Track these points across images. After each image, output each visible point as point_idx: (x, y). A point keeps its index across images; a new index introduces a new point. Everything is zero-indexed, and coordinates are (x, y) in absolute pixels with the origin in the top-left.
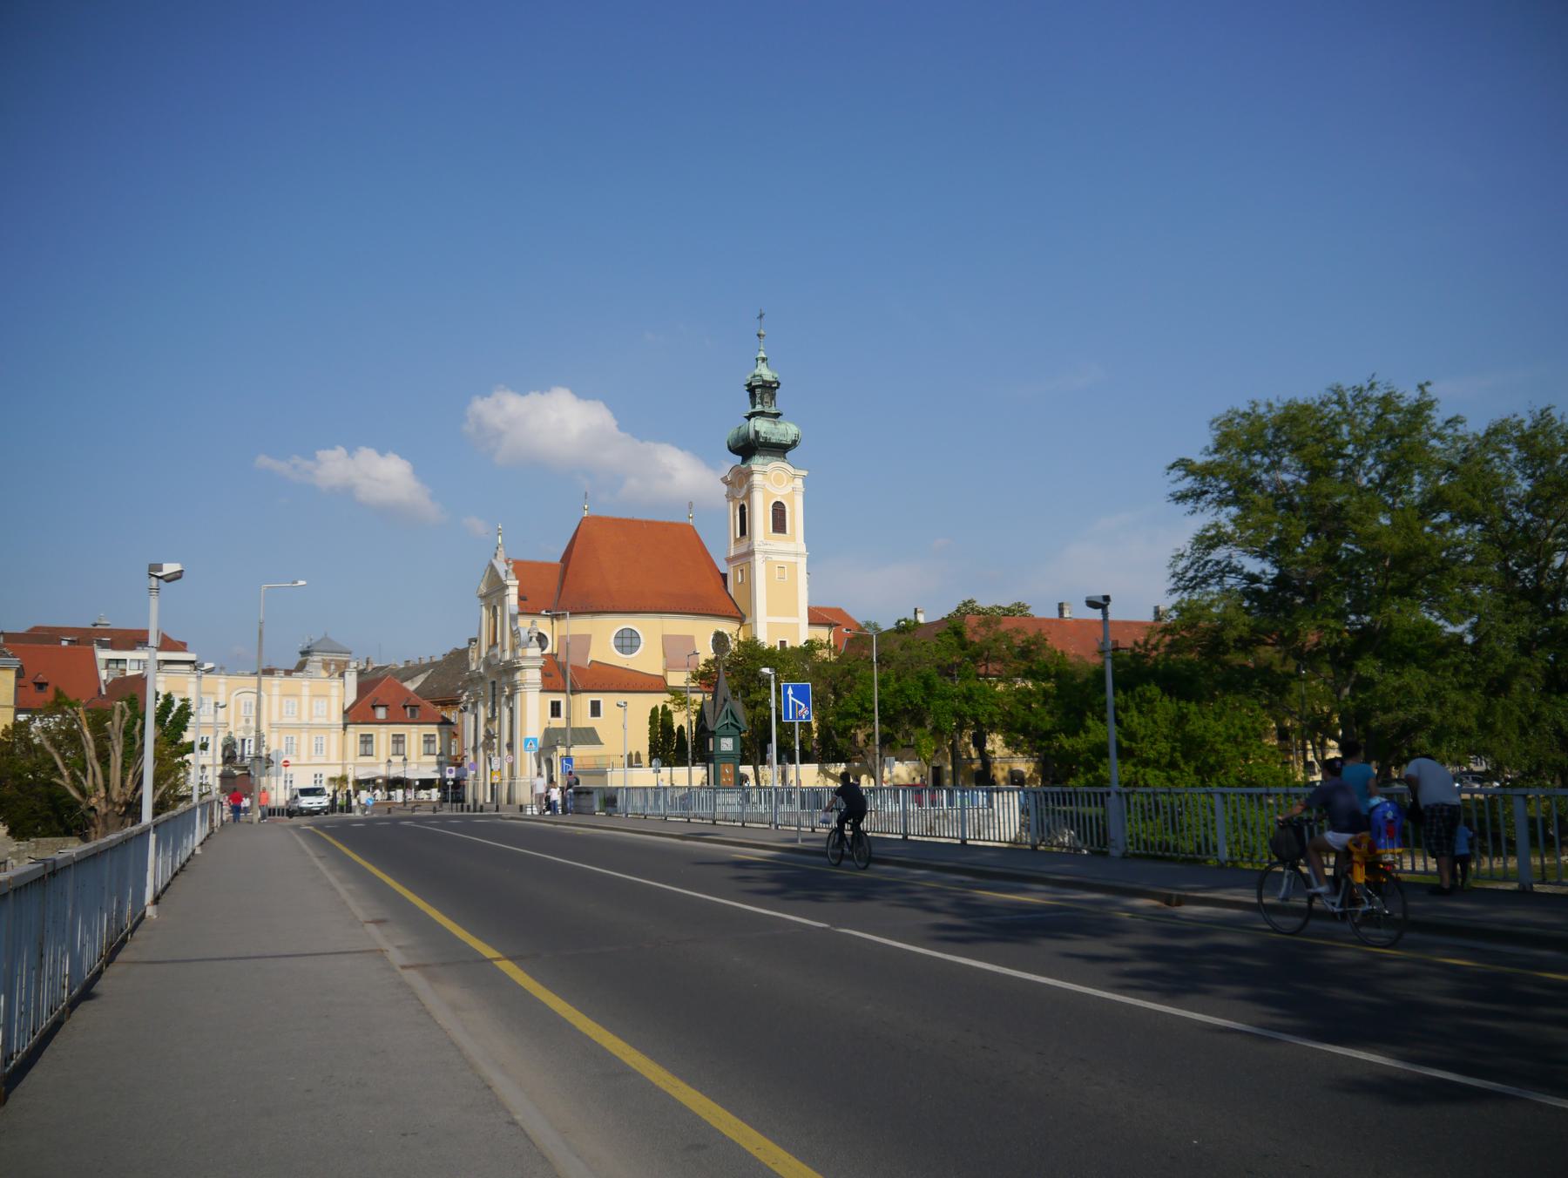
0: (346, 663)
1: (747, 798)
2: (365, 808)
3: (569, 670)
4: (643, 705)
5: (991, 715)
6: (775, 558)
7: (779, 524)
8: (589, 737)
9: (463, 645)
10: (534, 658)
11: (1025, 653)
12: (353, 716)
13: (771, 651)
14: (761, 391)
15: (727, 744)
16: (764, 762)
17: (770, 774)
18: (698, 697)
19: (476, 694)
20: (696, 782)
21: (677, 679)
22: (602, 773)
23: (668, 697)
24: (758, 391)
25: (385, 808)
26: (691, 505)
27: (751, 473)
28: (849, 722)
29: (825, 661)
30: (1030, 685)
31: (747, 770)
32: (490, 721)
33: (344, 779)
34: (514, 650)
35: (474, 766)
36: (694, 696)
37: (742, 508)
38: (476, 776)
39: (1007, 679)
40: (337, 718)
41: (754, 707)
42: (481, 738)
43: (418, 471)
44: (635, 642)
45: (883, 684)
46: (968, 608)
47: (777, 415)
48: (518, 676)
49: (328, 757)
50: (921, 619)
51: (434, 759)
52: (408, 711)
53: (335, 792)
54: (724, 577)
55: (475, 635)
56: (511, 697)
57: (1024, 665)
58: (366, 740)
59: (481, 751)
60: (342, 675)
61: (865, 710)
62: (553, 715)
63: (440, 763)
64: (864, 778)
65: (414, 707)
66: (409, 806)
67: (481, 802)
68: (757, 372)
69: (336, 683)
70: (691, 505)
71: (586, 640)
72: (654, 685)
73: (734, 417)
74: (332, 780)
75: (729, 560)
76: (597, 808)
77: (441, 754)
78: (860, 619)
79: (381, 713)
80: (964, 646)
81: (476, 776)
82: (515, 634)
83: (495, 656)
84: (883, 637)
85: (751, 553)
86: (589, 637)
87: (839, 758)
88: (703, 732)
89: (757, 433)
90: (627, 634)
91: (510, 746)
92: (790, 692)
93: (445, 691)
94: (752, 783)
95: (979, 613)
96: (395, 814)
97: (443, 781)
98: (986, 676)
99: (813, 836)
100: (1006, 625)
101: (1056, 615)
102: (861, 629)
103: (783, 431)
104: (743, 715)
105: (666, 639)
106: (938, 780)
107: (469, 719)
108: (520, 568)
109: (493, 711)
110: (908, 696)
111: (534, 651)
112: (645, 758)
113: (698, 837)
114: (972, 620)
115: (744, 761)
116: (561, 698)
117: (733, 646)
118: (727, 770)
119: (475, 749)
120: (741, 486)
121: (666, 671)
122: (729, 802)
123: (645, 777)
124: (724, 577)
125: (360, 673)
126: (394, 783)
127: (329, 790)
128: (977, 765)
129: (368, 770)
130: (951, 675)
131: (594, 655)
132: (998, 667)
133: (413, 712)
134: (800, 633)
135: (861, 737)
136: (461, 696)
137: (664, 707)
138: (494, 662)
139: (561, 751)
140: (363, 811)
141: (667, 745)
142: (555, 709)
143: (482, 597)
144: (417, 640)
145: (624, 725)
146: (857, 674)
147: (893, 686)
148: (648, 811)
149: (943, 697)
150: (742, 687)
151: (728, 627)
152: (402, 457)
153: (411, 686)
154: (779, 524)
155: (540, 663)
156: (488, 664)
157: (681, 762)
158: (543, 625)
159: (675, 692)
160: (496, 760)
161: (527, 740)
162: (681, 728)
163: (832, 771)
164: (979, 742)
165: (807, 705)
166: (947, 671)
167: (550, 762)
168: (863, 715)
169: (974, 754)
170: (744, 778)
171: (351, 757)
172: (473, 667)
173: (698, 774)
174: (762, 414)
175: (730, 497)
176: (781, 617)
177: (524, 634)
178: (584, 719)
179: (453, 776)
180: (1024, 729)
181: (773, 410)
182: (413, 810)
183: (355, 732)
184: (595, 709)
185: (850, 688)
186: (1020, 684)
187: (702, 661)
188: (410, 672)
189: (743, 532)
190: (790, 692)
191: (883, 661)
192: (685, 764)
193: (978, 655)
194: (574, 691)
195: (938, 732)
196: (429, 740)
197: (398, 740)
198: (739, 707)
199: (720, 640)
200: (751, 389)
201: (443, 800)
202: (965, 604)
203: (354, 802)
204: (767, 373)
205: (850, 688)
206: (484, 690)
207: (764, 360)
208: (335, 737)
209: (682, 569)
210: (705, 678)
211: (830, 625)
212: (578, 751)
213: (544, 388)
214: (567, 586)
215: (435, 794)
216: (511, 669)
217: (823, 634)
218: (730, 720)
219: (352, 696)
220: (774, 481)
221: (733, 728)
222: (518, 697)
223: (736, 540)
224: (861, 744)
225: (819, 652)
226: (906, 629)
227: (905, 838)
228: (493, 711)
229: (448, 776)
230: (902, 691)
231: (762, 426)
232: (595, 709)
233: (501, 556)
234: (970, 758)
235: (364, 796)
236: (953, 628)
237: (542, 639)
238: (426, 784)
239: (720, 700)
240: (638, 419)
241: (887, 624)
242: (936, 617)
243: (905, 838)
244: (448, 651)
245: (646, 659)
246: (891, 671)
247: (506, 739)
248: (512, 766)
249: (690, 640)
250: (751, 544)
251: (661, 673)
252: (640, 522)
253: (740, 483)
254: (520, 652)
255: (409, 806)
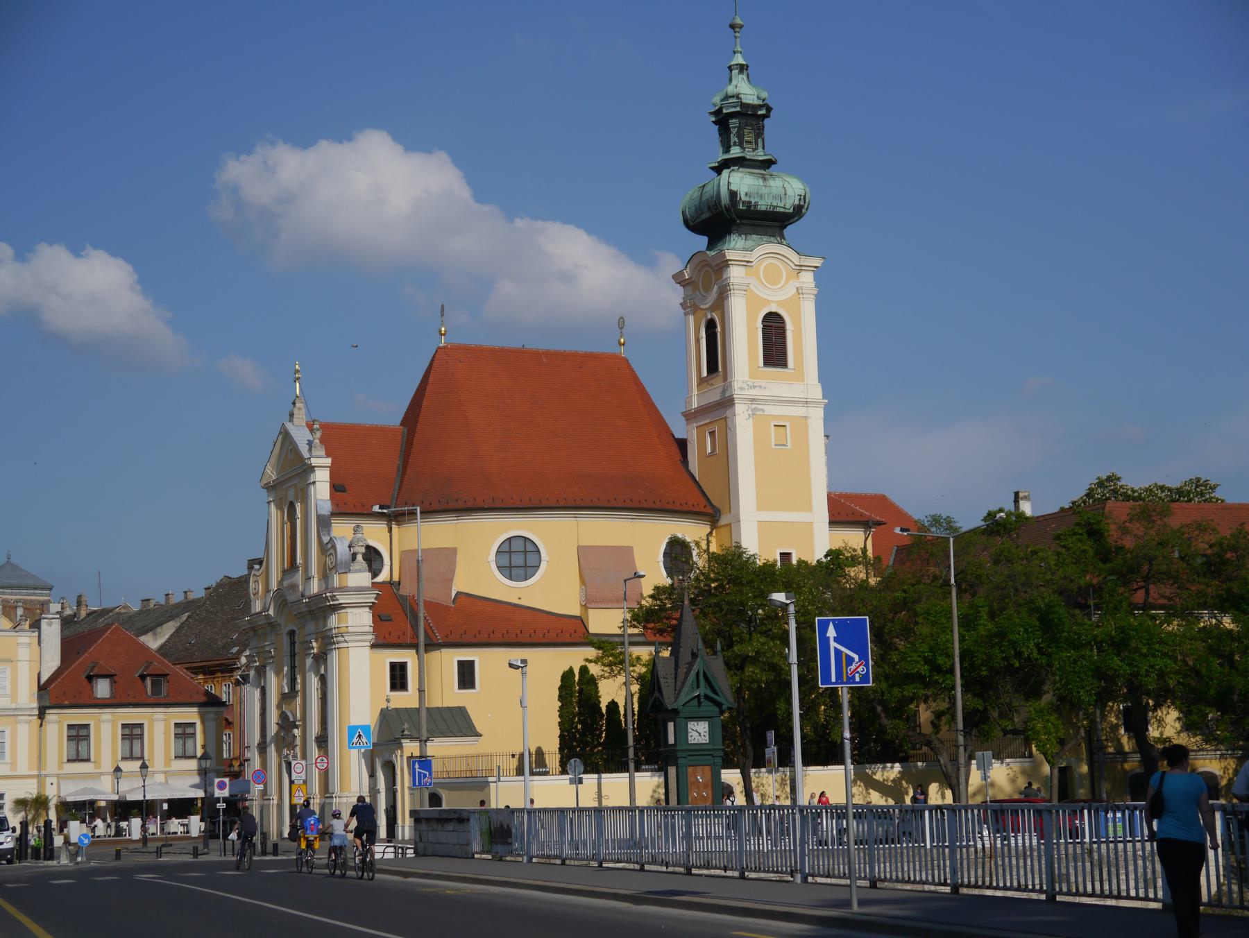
0: (44, 606)
1: (734, 824)
2: (74, 850)
3: (422, 613)
4: (550, 665)
5: (1162, 675)
6: (770, 410)
7: (775, 348)
8: (456, 723)
9: (239, 571)
10: (359, 590)
11: (1215, 566)
12: (52, 695)
13: (768, 568)
14: (739, 123)
15: (699, 732)
16: (760, 762)
17: (769, 784)
18: (645, 653)
19: (262, 653)
20: (643, 800)
21: (606, 622)
22: (483, 785)
23: (591, 652)
24: (734, 123)
25: (112, 850)
26: (621, 323)
27: (725, 264)
28: (909, 690)
29: (863, 586)
30: (1227, 622)
31: (731, 776)
32: (286, 698)
33: (40, 803)
34: (325, 576)
35: (262, 775)
36: (637, 651)
37: (711, 325)
38: (264, 793)
39: (1186, 614)
40: (27, 698)
41: (741, 668)
42: (273, 729)
43: (150, 282)
44: (531, 559)
45: (966, 622)
46: (1108, 484)
47: (767, 164)
48: (333, 621)
49: (13, 765)
50: (1026, 508)
51: (193, 765)
52: (147, 685)
53: (24, 825)
54: (682, 444)
55: (259, 554)
56: (322, 658)
57: (1213, 588)
58: (79, 734)
59: (272, 751)
60: (36, 625)
61: (936, 669)
62: (394, 687)
63: (203, 772)
64: (933, 788)
65: (159, 678)
66: (152, 846)
67: (273, 837)
68: (731, 89)
69: (26, 638)
70: (621, 323)
71: (449, 555)
72: (568, 632)
73: (691, 166)
74: (21, 804)
75: (690, 416)
76: (476, 846)
77: (205, 757)
78: (918, 510)
79: (103, 689)
80: (1105, 555)
81: (264, 793)
82: (327, 549)
83: (294, 587)
84: (966, 540)
85: (727, 402)
86: (454, 551)
87: (886, 757)
88: (654, 706)
89: (733, 195)
90: (517, 546)
91: (323, 741)
92: (831, 632)
93: (217, 651)
94: (740, 800)
95: (1128, 498)
96: (128, 860)
97: (209, 801)
98: (1146, 606)
99: (873, 894)
100: (1179, 518)
101: (1010, 506)
102: (922, 528)
103: (782, 189)
104: (725, 682)
105: (584, 553)
106: (1065, 791)
107: (252, 695)
108: (334, 437)
109: (293, 681)
110: (1013, 644)
111: (359, 578)
112: (553, 760)
113: (663, 898)
114: (1118, 511)
115: (729, 765)
116: (407, 657)
117: (700, 561)
118: (700, 776)
119: (262, 747)
120: (708, 289)
121: (585, 607)
122: (710, 833)
123: (555, 791)
124: (682, 444)
125: (66, 622)
126: (123, 809)
127: (14, 821)
128: (1133, 764)
129: (82, 785)
130: (1084, 607)
131: (463, 583)
132: (1168, 592)
133: (156, 685)
134: (817, 540)
135: (925, 715)
136: (237, 657)
137: (584, 670)
138: (291, 598)
139: (411, 748)
140: (73, 856)
141: (590, 738)
142: (398, 677)
143: (270, 488)
144: (161, 563)
145: (515, 703)
146: (919, 608)
147: (986, 626)
148: (567, 851)
149: (1076, 645)
150: (719, 633)
151: (692, 531)
152: (113, 253)
153: (153, 642)
154: (775, 348)
155: (371, 598)
156: (281, 599)
157: (618, 765)
158: (375, 534)
159: (603, 643)
160: (298, 766)
161: (352, 729)
162: (613, 705)
163: (878, 777)
164: (1136, 723)
165: (863, 657)
166: (1078, 600)
167: (390, 768)
168: (933, 678)
169: (1127, 743)
170: (729, 791)
171: (52, 765)
172: (257, 607)
173: (648, 785)
174: (741, 162)
175: (689, 306)
176: (782, 511)
177: (342, 549)
178: (447, 693)
179: (226, 793)
180: (1222, 702)
181: (760, 155)
182: (159, 853)
183: (59, 721)
184: (466, 675)
185: (906, 632)
186: (1206, 620)
187: (648, 590)
188: (151, 618)
189: (713, 367)
190: (831, 632)
191: (967, 585)
192: (621, 767)
193: (1135, 570)
194: (432, 646)
195: (1066, 705)
196: (183, 732)
197: (132, 733)
198: (717, 666)
199: (677, 552)
200: (722, 120)
201: (210, 834)
202: (1101, 484)
203: (58, 841)
204: (746, 90)
205: (906, 632)
206: (277, 645)
207: (742, 68)
208: (24, 731)
209: (611, 434)
210: (655, 619)
211: (866, 524)
212: (439, 748)
213: (343, 133)
214: (412, 467)
215: (196, 824)
216: (322, 608)
217: (854, 539)
218: (703, 690)
219: (52, 661)
220: (764, 278)
221: (706, 705)
222: (334, 657)
223: (701, 381)
224: (927, 729)
225: (852, 571)
226: (1000, 527)
227: (1051, 898)
228: (293, 681)
229: (218, 793)
230: (1002, 635)
231: (741, 182)
232: (466, 675)
233: (301, 416)
234: (1120, 750)
235: (76, 829)
236: (1087, 522)
237: (372, 557)
238: (181, 808)
239: (685, 657)
240: (509, 178)
241: (970, 519)
242: (1052, 508)
243: (1051, 898)
244: (213, 582)
245: (553, 589)
246: (980, 601)
247: (314, 729)
248: (325, 776)
249: (625, 554)
250: (727, 386)
251: (576, 612)
252: (536, 355)
253: (705, 285)
254: (336, 580)
255: (152, 846)
